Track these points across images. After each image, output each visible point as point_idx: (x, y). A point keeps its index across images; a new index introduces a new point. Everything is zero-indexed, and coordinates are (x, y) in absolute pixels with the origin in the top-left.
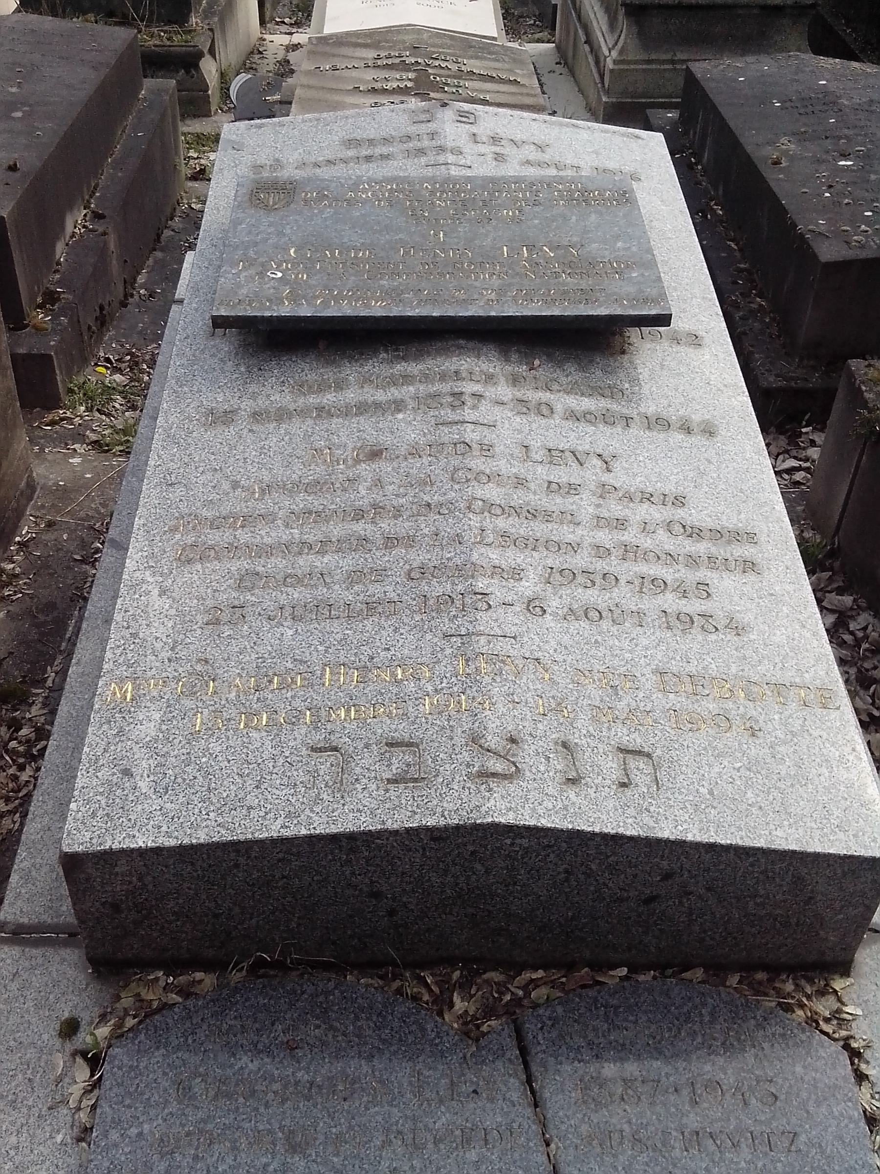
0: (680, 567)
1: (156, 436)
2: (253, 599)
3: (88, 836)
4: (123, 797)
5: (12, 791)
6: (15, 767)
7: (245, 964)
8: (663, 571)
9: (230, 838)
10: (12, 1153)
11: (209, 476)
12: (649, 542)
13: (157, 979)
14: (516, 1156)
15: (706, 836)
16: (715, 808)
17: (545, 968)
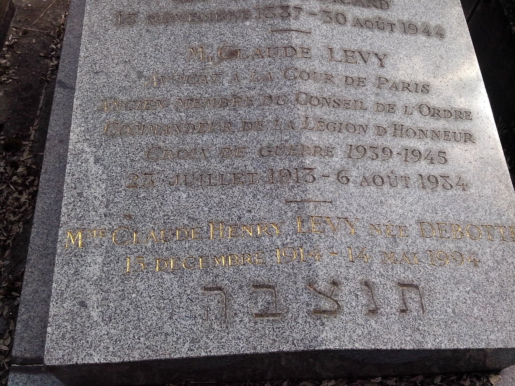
0: (428, 140)
1: (84, 32)
2: (158, 168)
3: (61, 354)
4: (82, 324)
5: (17, 208)
6: (17, 193)
8: (419, 144)
9: (155, 358)
11: (121, 66)
12: (409, 121)
15: (452, 345)
16: (456, 323)
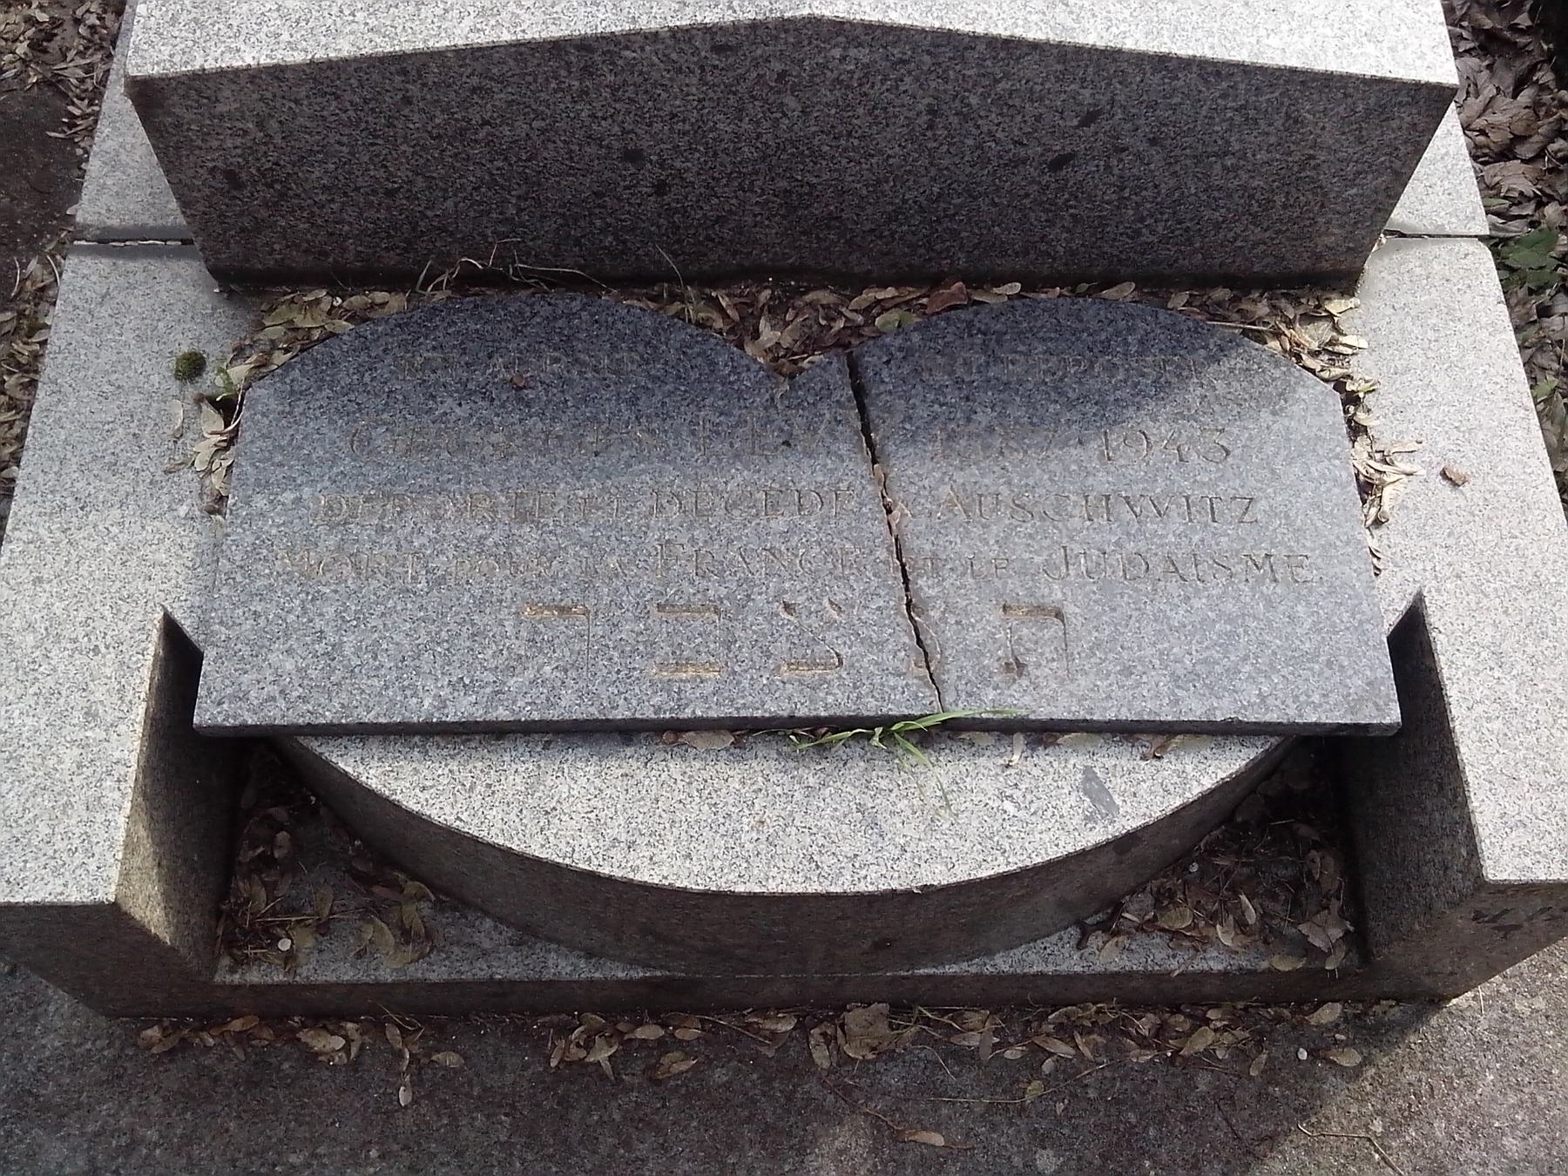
7: (445, 278)
10: (115, 530)
13: (318, 301)
14: (843, 525)
17: (898, 282)
